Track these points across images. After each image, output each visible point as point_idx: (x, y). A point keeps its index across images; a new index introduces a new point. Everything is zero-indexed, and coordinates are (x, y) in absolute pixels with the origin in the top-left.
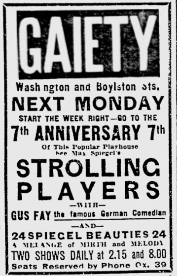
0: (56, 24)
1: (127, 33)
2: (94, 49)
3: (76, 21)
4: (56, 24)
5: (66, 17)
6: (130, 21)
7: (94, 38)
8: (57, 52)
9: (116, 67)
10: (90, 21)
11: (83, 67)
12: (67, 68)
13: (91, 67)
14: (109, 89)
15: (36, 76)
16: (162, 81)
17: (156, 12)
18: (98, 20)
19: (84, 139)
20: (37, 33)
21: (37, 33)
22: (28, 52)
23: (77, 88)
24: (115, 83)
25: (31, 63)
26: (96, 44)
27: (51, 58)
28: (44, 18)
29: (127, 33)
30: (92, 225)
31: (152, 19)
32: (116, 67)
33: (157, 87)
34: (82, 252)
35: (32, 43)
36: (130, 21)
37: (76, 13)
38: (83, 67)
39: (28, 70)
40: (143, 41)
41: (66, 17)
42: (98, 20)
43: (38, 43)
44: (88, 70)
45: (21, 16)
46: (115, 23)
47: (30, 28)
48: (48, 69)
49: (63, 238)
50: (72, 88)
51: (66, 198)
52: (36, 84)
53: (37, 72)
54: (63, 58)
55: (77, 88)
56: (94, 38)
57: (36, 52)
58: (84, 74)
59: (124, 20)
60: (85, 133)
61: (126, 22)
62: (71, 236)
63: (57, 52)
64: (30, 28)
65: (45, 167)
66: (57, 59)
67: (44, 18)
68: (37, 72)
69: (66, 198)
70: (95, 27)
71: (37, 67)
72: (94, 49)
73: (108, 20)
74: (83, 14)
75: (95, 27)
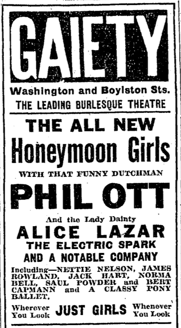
0: (53, 27)
1: (132, 31)
2: (93, 52)
3: (74, 21)
4: (53, 27)
5: (64, 19)
6: (135, 20)
7: (93, 40)
8: (54, 55)
9: (121, 71)
10: (88, 22)
11: (83, 73)
12: (65, 73)
13: (90, 72)
14: (116, 92)
15: (31, 80)
16: (169, 85)
17: (164, 13)
18: (99, 20)
19: (141, 107)
20: (31, 35)
21: (31, 35)
22: (22, 57)
23: (81, 92)
24: (123, 87)
25: (24, 65)
26: (96, 46)
27: (47, 62)
28: (40, 19)
29: (132, 31)
30: (53, 275)
31: (161, 20)
32: (121, 71)
33: (168, 90)
34: (149, 160)
35: (26, 45)
36: (135, 20)
37: (74, 14)
38: (83, 73)
39: (20, 74)
40: (152, 44)
41: (64, 19)
42: (99, 20)
43: (36, 45)
44: (86, 76)
45: (13, 16)
46: (120, 23)
47: (24, 30)
48: (44, 74)
49: (63, 236)
50: (77, 91)
51: (22, 238)
52: (35, 88)
53: (32, 77)
54: (61, 61)
55: (81, 92)
56: (93, 40)
57: (30, 56)
58: (82, 79)
59: (130, 20)
60: (142, 104)
61: (132, 22)
62: (76, 232)
63: (54, 55)
64: (24, 30)
65: (155, 103)
66: (54, 63)
67: (40, 19)
68: (32, 77)
69: (22, 238)
70: (94, 27)
71: (32, 71)
72: (93, 52)
73: (110, 20)
74: (81, 15)
75: (94, 27)
